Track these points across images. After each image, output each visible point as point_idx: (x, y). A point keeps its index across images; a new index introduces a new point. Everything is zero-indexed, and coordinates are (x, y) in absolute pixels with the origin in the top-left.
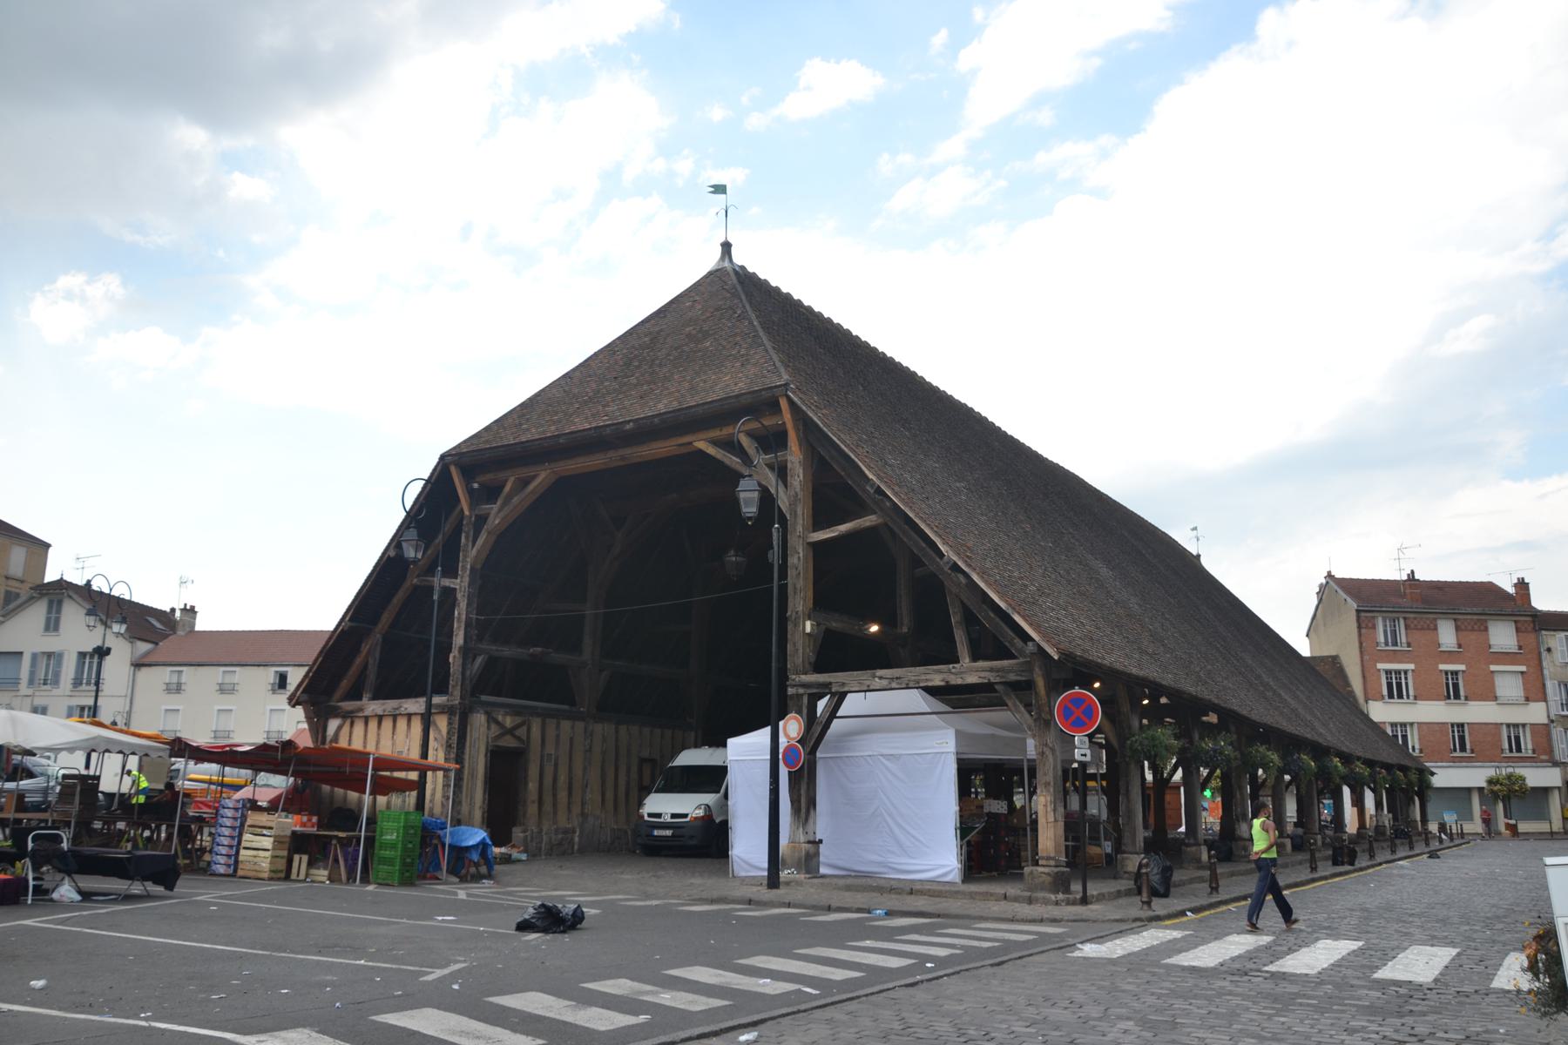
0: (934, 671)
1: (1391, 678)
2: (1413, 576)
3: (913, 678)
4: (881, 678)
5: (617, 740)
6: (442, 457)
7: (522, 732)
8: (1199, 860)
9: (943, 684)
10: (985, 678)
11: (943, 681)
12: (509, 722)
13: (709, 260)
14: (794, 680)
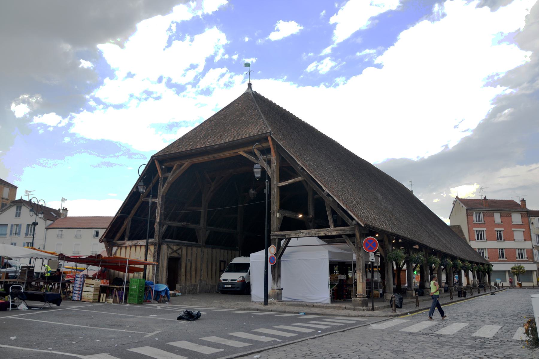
4: (303, 233)
5: (212, 254)
8: (412, 296)
9: (324, 235)
12: (175, 248)
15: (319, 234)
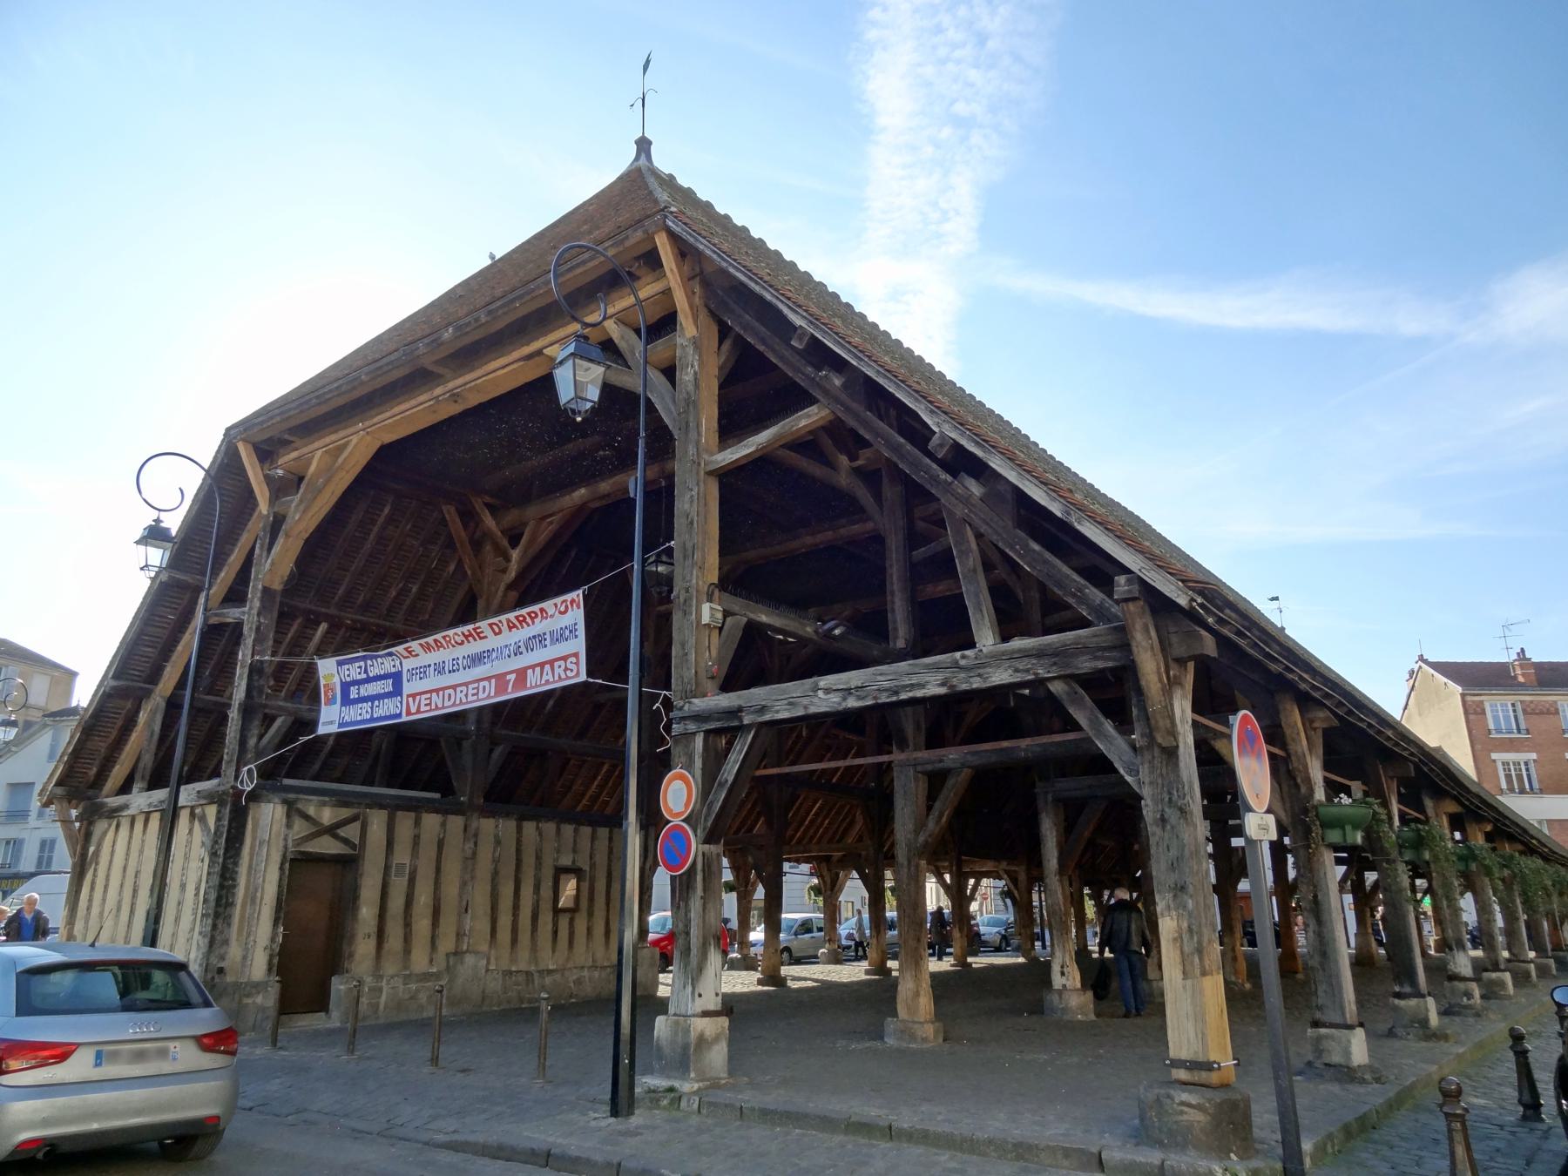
0: (927, 666)
1: (1510, 770)
2: (1524, 655)
3: (887, 684)
4: (828, 691)
5: (519, 841)
6: (228, 430)
7: (351, 832)
8: (1424, 1022)
9: (942, 691)
10: (1027, 671)
11: (942, 685)
12: (327, 816)
13: (619, 162)
14: (681, 709)
15: (912, 687)
